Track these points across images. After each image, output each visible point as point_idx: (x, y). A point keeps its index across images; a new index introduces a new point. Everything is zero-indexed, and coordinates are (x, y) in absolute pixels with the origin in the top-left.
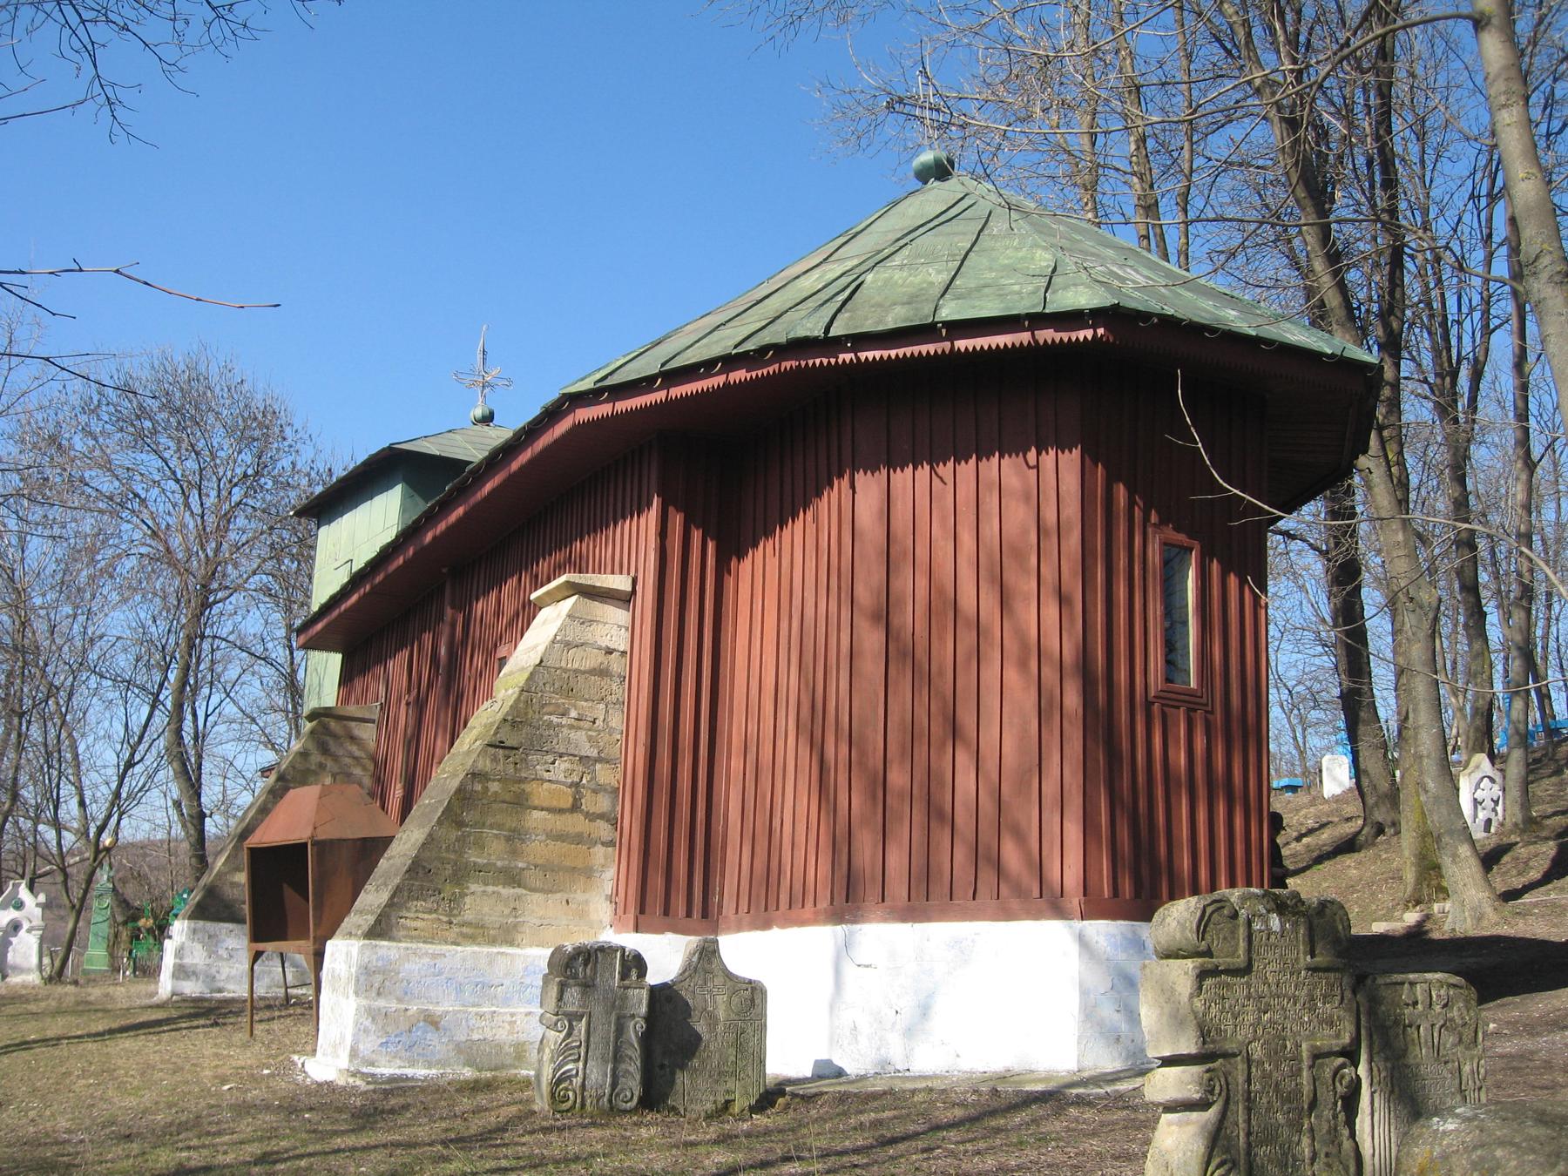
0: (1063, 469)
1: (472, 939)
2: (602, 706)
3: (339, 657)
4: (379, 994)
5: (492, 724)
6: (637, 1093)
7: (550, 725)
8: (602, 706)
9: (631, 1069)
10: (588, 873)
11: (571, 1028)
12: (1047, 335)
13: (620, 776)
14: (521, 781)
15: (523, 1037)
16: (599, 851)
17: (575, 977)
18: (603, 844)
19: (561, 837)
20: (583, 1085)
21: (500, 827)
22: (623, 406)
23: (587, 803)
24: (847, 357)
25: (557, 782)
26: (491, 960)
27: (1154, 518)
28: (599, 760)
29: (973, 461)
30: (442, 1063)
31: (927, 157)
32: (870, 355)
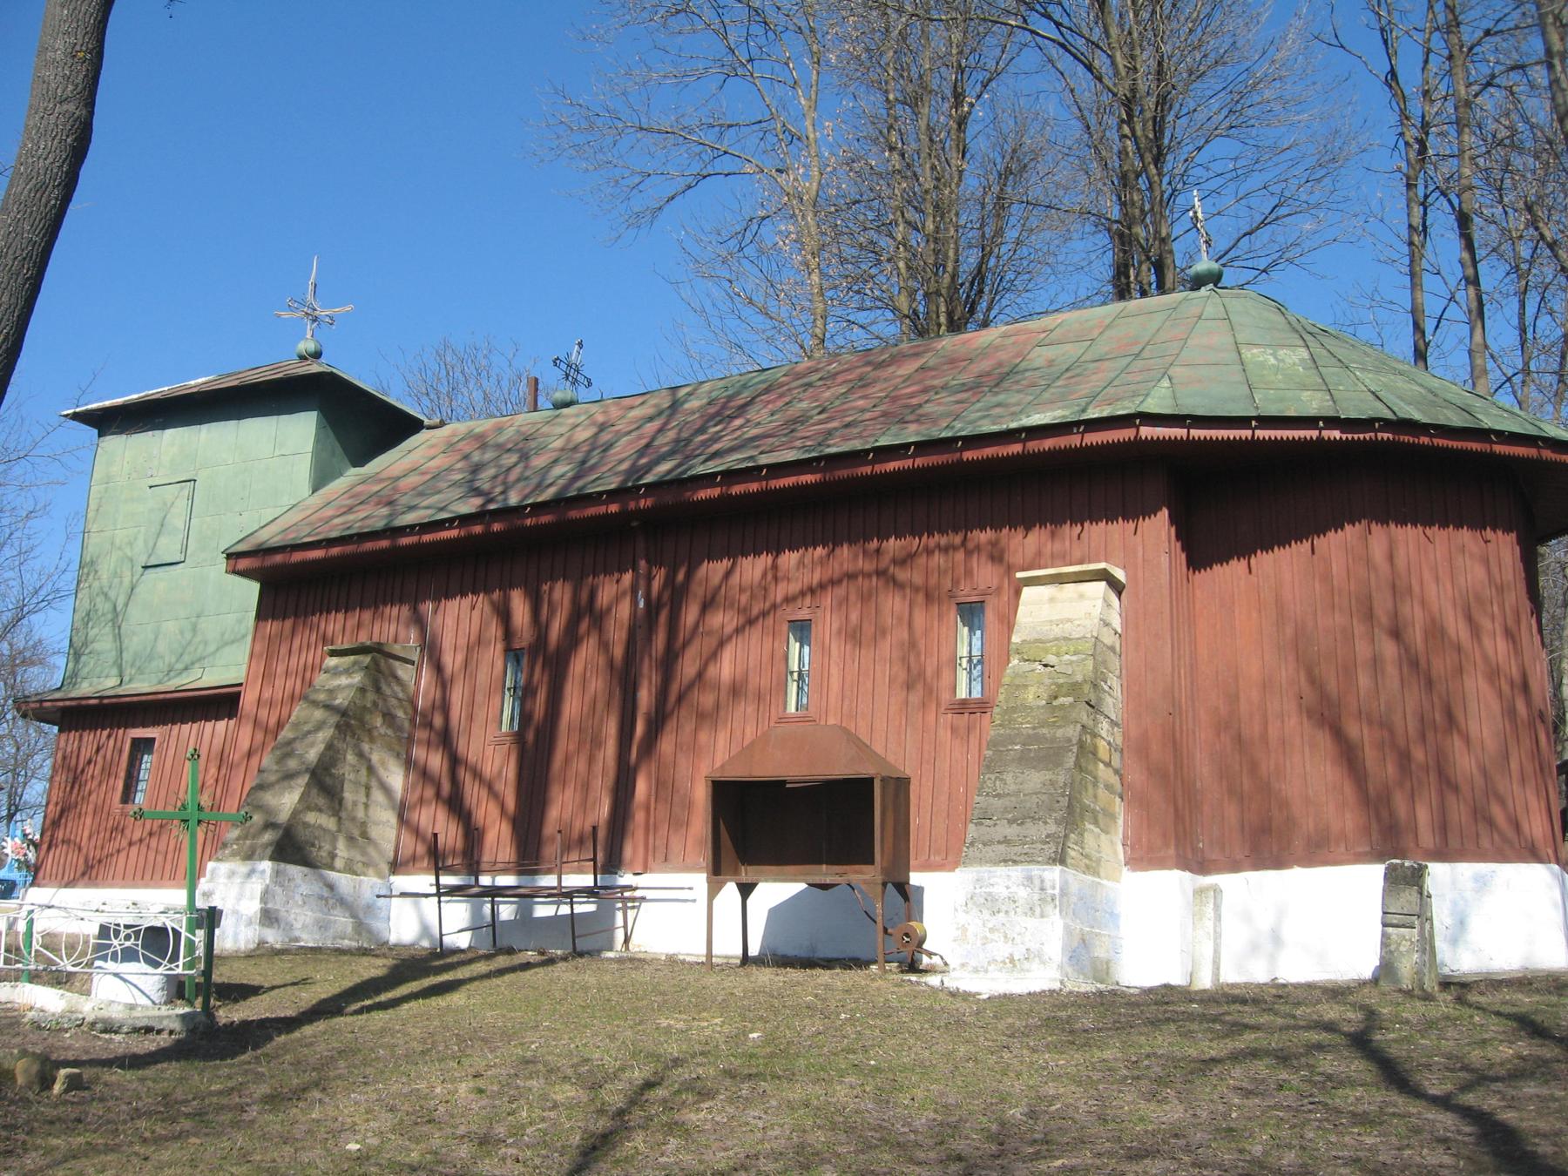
22: (1196, 433)
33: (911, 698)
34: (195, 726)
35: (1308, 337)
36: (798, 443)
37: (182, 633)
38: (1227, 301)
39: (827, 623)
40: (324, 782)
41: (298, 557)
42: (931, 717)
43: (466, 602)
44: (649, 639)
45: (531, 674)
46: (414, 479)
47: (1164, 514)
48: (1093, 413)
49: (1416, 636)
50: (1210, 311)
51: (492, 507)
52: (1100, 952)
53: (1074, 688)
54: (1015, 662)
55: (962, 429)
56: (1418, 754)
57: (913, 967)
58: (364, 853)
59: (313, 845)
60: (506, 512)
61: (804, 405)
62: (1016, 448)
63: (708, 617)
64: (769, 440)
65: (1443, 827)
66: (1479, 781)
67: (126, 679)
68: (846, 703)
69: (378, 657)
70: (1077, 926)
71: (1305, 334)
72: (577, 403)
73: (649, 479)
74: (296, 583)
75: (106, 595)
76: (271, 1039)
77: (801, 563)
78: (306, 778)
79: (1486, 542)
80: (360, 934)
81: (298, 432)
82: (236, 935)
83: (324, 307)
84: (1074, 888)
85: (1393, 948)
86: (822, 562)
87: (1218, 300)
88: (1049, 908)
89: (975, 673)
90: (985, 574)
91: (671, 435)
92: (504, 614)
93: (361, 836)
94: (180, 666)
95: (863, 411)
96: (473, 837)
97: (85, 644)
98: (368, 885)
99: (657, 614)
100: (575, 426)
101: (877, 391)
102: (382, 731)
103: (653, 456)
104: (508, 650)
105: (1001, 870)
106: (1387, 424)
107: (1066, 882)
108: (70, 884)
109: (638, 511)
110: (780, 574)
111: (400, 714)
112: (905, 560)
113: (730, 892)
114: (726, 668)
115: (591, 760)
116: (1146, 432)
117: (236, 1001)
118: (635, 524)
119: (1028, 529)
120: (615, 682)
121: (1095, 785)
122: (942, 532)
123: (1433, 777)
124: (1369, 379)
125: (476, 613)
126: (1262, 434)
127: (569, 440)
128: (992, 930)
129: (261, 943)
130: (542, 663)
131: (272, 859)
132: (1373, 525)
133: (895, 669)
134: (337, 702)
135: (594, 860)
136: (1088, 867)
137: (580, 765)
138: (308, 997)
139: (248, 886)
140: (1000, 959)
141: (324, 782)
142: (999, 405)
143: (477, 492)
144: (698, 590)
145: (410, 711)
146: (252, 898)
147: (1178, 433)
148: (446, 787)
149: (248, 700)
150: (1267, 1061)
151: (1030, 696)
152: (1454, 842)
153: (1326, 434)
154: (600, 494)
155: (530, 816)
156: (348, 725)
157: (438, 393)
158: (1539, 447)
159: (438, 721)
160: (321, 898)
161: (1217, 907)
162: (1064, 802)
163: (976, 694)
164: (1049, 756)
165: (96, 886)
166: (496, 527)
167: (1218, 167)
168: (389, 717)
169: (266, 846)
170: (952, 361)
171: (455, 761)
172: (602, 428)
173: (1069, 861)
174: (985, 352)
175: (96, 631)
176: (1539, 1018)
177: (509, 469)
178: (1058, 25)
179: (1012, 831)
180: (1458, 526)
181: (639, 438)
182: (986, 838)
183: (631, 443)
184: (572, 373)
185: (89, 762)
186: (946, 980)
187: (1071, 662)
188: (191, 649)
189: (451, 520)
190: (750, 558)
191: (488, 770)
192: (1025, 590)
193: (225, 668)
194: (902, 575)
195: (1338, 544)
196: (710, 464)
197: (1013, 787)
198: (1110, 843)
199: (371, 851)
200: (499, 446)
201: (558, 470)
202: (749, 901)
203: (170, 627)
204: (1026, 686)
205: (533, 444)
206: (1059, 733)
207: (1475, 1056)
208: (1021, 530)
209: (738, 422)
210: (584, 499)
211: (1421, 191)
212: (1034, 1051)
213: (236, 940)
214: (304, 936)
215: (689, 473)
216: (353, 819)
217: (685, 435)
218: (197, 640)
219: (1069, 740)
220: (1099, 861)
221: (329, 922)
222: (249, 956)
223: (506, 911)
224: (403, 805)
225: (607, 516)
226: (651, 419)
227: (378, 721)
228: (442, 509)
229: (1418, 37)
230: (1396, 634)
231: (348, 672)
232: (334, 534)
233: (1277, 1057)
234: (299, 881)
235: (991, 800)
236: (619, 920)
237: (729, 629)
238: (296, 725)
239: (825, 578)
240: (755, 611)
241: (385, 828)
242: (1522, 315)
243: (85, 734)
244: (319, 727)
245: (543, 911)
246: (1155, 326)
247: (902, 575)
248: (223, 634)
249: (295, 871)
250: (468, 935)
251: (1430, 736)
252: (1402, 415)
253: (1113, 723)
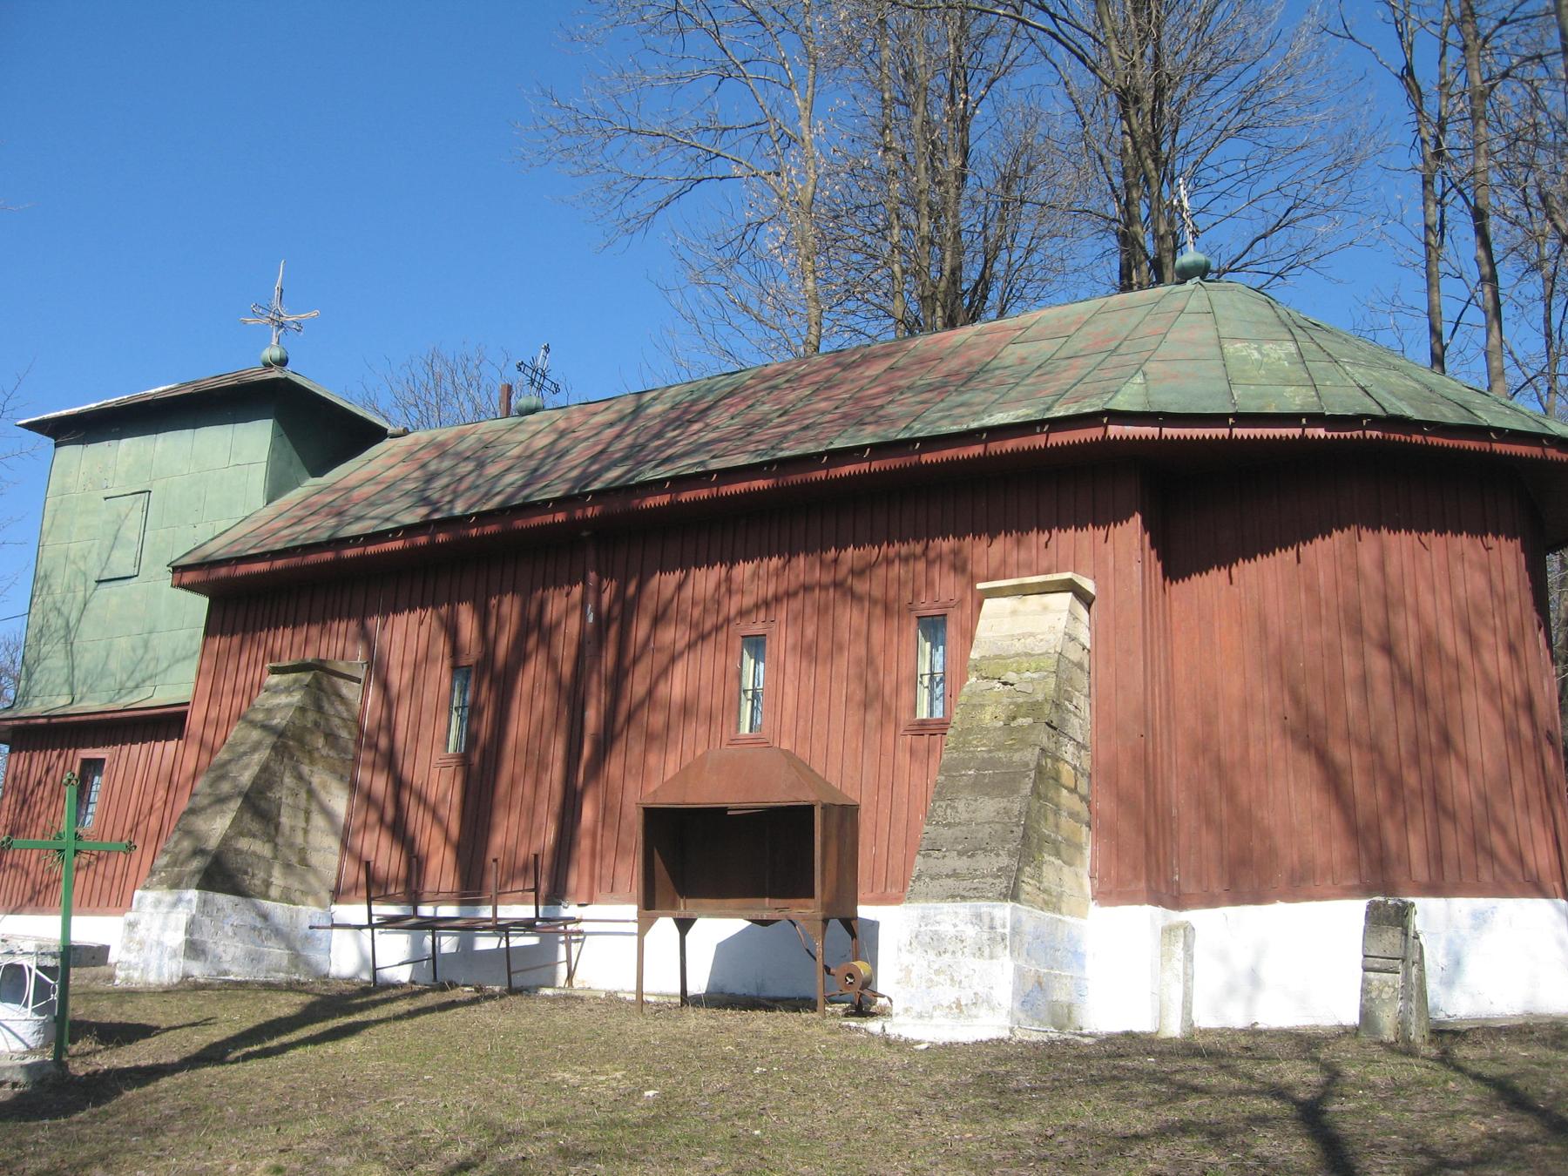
3: (207, 600)
22: (1169, 432)
33: (868, 718)
34: (145, 746)
35: (1297, 332)
36: (751, 447)
37: (134, 650)
38: (1213, 294)
39: (782, 638)
40: (258, 806)
41: (243, 570)
42: (889, 741)
43: (414, 617)
44: (598, 655)
45: (477, 693)
46: (369, 489)
47: (1136, 520)
48: (1059, 412)
49: (1409, 651)
50: (1193, 304)
51: (436, 516)
52: (1060, 995)
53: (1034, 708)
54: (973, 680)
55: (920, 430)
56: (1411, 778)
57: (861, 1010)
58: (303, 881)
59: (246, 873)
60: (452, 522)
61: (766, 408)
62: (977, 450)
63: (659, 632)
64: (725, 446)
65: (1436, 857)
66: (1479, 808)
67: (77, 697)
68: (801, 723)
69: (320, 675)
70: (1032, 967)
71: (1291, 328)
72: (543, 409)
73: (596, 486)
74: (247, 596)
75: (59, 611)
76: (120, 1093)
77: (755, 574)
78: (239, 801)
79: (1488, 549)
80: (296, 966)
81: (255, 439)
82: (160, 967)
83: (291, 313)
84: (1028, 926)
85: (1374, 995)
86: (778, 573)
87: (1204, 293)
88: (999, 949)
89: (938, 691)
90: (947, 585)
91: (628, 440)
92: (451, 629)
93: (299, 863)
94: (131, 684)
95: (823, 413)
96: (415, 863)
97: (38, 660)
98: (308, 913)
99: (608, 628)
100: (536, 433)
101: (842, 393)
102: (324, 752)
103: (605, 463)
104: (455, 668)
105: (947, 907)
106: (1376, 422)
107: (1019, 921)
108: (17, 910)
109: (585, 521)
110: (734, 587)
111: (344, 734)
112: (858, 573)
113: (665, 927)
114: (676, 686)
115: (537, 783)
116: (1115, 431)
117: (119, 1044)
118: (585, 534)
119: (992, 537)
120: (563, 701)
121: (1057, 813)
122: (903, 540)
123: (1428, 806)
124: (1361, 375)
125: (424, 629)
126: (1239, 432)
127: (527, 448)
128: (937, 972)
129: (186, 976)
130: (488, 680)
131: (198, 887)
132: (1363, 531)
133: (852, 687)
134: (275, 722)
135: (536, 889)
136: (1046, 903)
137: (525, 789)
138: (200, 1040)
139: (173, 916)
140: (946, 1004)
141: (258, 806)
142: (961, 405)
143: (425, 501)
144: (649, 605)
145: (355, 731)
146: (176, 929)
147: (1150, 431)
148: (390, 813)
149: (195, 719)
150: (1199, 1138)
151: (986, 717)
152: (1450, 875)
153: (1310, 432)
154: (547, 502)
155: (466, 846)
156: (285, 746)
157: (427, 404)
158: (1543, 446)
159: (383, 742)
160: (254, 928)
161: (1188, 948)
162: (1019, 831)
163: (938, 714)
164: (1004, 783)
165: (42, 912)
166: (441, 538)
167: (1227, 169)
168: (331, 738)
169: (193, 874)
170: (922, 361)
171: (399, 783)
172: (562, 434)
173: (1023, 896)
174: (955, 351)
175: (48, 647)
176: (1519, 1084)
177: (462, 478)
178: (1053, 16)
179: (962, 864)
180: (1457, 531)
181: (595, 445)
182: (933, 872)
183: (588, 448)
184: (538, 378)
185: (39, 783)
186: (887, 1026)
187: (1033, 680)
188: (143, 666)
189: (395, 531)
190: (704, 570)
191: (432, 795)
192: (987, 602)
193: (174, 686)
194: (861, 587)
195: (1324, 552)
196: (661, 469)
197: (965, 816)
198: (1075, 876)
199: (311, 878)
200: (457, 454)
201: (511, 478)
202: (688, 937)
203: (123, 643)
204: (983, 706)
205: (491, 452)
206: (1016, 757)
207: (1440, 1134)
208: (985, 539)
209: (696, 427)
210: (529, 508)
211: (1438, 190)
212: (947, 1117)
213: (160, 974)
214: (235, 969)
215: (637, 479)
216: (291, 845)
217: (641, 440)
218: (148, 657)
219: (1027, 765)
220: (1060, 896)
221: (262, 954)
222: (167, 991)
223: (448, 944)
224: (346, 829)
225: (555, 525)
226: (611, 424)
227: (320, 742)
228: (388, 520)
229: (1435, 30)
230: (1388, 649)
231: (288, 690)
232: (278, 546)
233: (1211, 1133)
234: (229, 911)
235: (941, 830)
236: (562, 955)
237: (680, 645)
238: (232, 746)
239: (781, 590)
240: (708, 625)
241: (326, 854)
242: (1548, 320)
243: (36, 754)
244: (255, 748)
245: (486, 943)
246: (1134, 320)
247: (861, 587)
248: (174, 651)
249: (222, 899)
250: (408, 969)
251: (1425, 758)
252: (1391, 411)
253: (1080, 746)
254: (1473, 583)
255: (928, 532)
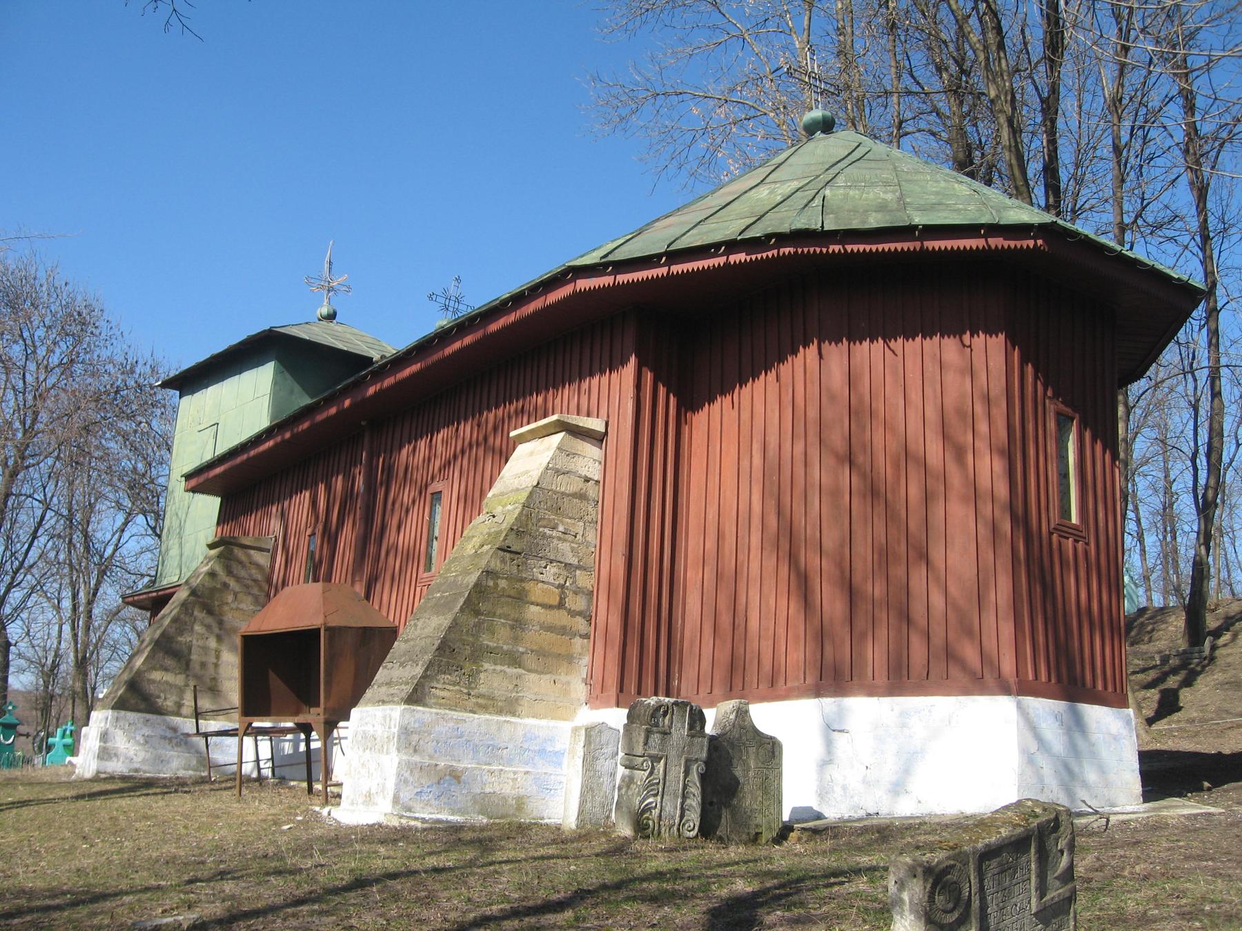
0: (990, 353)
1: (484, 708)
2: (581, 524)
3: (219, 499)
4: (415, 751)
5: (498, 533)
6: (697, 824)
7: (544, 536)
8: (581, 524)
9: (694, 804)
10: (569, 659)
11: (653, 768)
12: (996, 242)
13: (594, 581)
14: (522, 580)
15: (522, 792)
16: (578, 642)
17: (657, 725)
18: (581, 636)
19: (550, 629)
20: (660, 816)
21: (506, 617)
22: (623, 278)
23: (569, 603)
24: (836, 248)
25: (548, 583)
26: (500, 726)
27: (1049, 393)
28: (579, 567)
29: (918, 339)
30: (461, 812)
31: (817, 114)
32: (855, 248)
116: (584, 284)
118: (363, 423)
147: (607, 281)
254: (957, 387)
255: (524, 393)
